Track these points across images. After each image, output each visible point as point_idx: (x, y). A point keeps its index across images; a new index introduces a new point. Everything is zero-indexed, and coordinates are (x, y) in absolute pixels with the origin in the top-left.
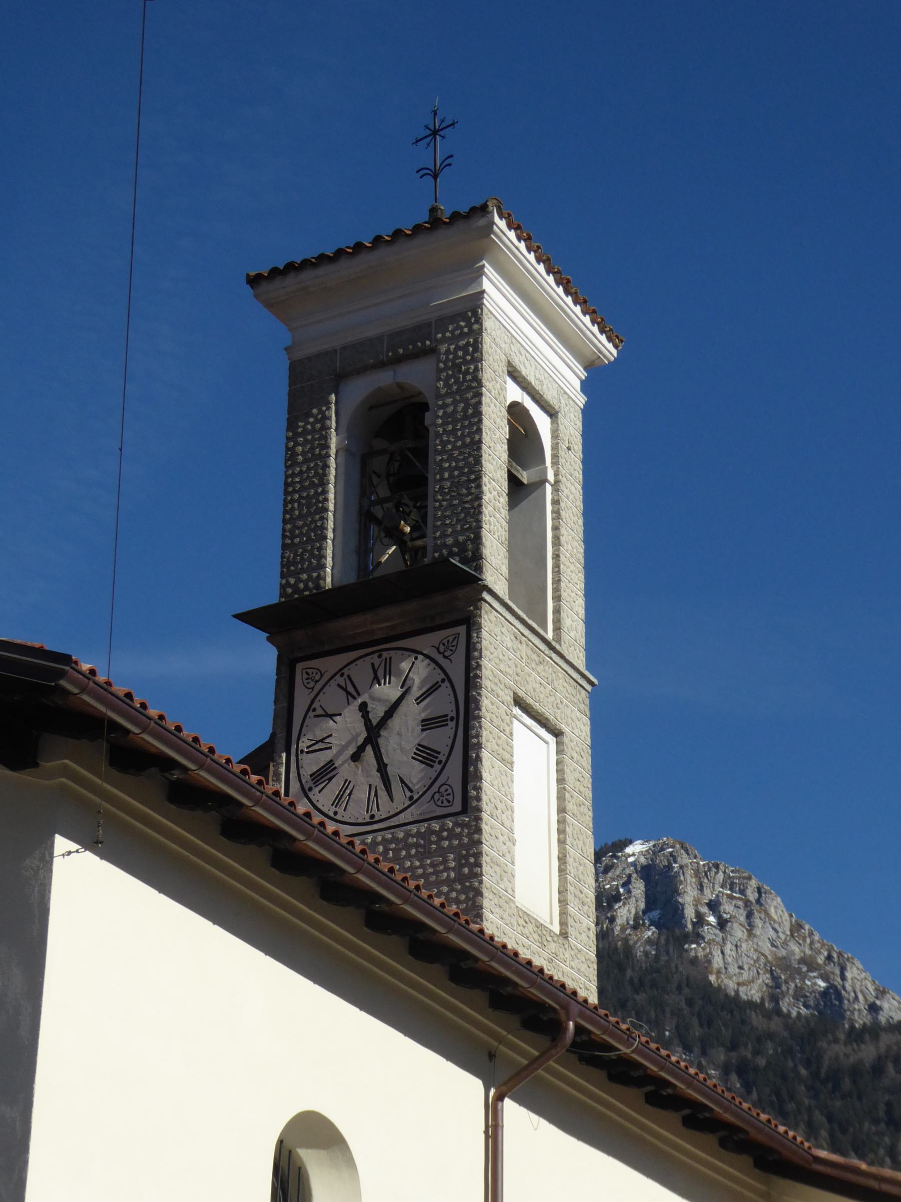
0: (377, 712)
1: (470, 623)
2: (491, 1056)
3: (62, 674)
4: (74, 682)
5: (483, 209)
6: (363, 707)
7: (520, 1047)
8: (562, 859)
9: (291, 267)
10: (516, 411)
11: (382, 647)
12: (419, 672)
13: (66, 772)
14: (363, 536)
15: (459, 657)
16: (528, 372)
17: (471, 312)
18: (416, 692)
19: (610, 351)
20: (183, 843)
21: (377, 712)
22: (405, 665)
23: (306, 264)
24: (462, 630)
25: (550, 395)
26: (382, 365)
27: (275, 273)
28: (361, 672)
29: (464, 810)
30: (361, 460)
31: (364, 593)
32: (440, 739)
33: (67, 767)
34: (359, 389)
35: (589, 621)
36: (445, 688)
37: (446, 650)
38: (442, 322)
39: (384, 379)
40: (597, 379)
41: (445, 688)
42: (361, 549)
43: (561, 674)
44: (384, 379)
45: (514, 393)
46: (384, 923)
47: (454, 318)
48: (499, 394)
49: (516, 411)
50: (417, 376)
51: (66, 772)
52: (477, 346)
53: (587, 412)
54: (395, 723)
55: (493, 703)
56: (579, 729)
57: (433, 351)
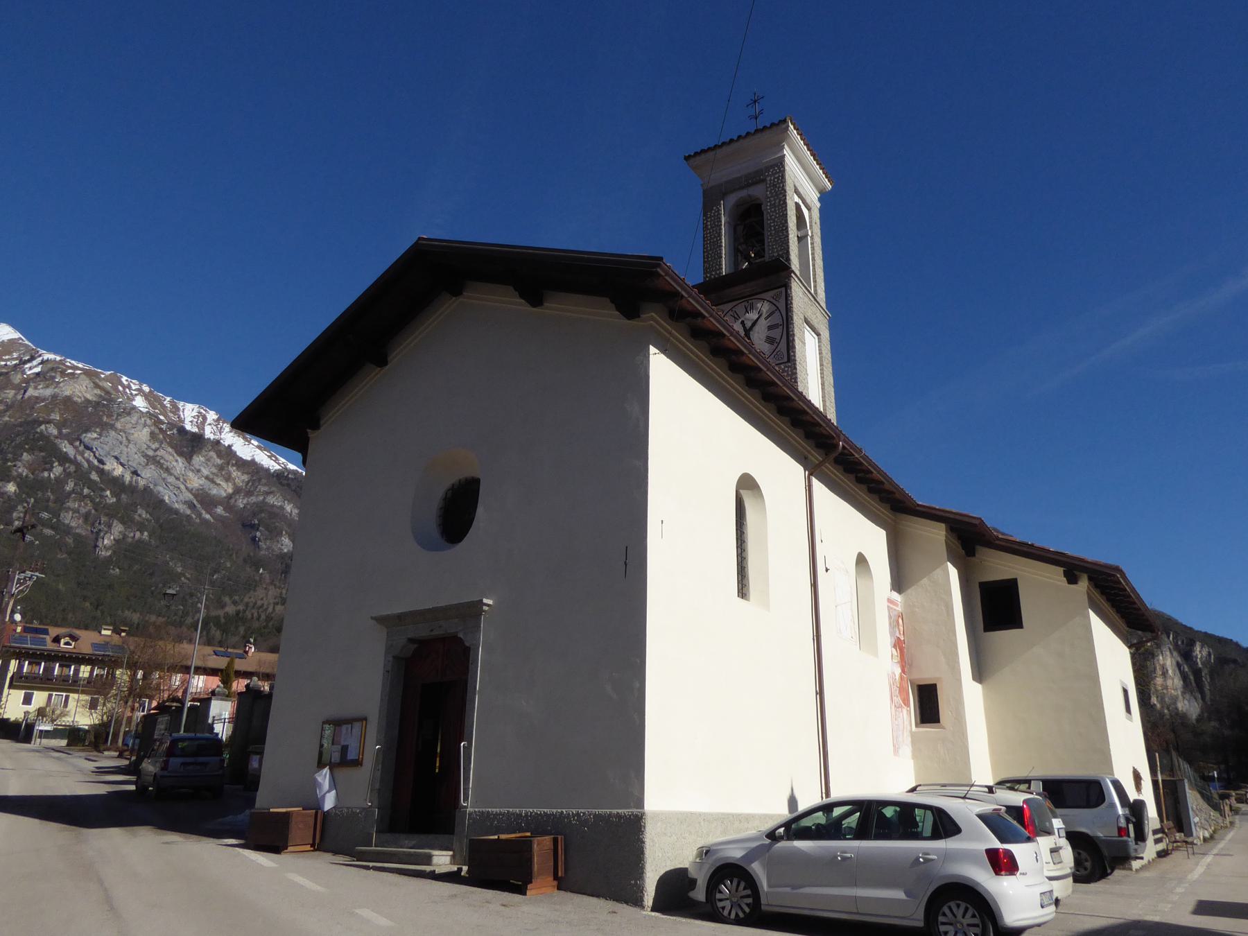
0: (748, 324)
1: (787, 286)
2: (806, 458)
3: (659, 265)
4: (663, 270)
5: (785, 121)
6: (743, 323)
7: (816, 456)
8: (823, 384)
9: (703, 151)
10: (797, 205)
11: (748, 299)
12: (765, 308)
13: (653, 319)
14: (736, 256)
15: (783, 301)
16: (800, 190)
17: (780, 164)
18: (764, 315)
19: (829, 186)
20: (697, 356)
21: (748, 324)
22: (759, 305)
23: (709, 149)
24: (783, 289)
25: (808, 201)
26: (742, 188)
27: (696, 154)
28: (740, 309)
29: (789, 361)
30: (734, 227)
31: (735, 278)
32: (776, 333)
33: (653, 317)
34: (733, 199)
35: (826, 291)
36: (777, 314)
37: (776, 298)
38: (767, 169)
39: (743, 193)
40: (824, 197)
41: (777, 314)
42: (735, 263)
43: (24, 754)
44: (743, 193)
45: (797, 199)
46: (763, 393)
47: (772, 166)
48: (792, 199)
49: (797, 205)
50: (757, 191)
51: (653, 319)
52: (783, 177)
53: (821, 210)
54: (756, 328)
55: (797, 319)
56: (826, 334)
57: (764, 181)
